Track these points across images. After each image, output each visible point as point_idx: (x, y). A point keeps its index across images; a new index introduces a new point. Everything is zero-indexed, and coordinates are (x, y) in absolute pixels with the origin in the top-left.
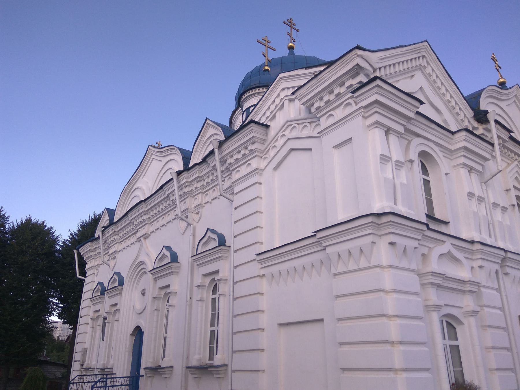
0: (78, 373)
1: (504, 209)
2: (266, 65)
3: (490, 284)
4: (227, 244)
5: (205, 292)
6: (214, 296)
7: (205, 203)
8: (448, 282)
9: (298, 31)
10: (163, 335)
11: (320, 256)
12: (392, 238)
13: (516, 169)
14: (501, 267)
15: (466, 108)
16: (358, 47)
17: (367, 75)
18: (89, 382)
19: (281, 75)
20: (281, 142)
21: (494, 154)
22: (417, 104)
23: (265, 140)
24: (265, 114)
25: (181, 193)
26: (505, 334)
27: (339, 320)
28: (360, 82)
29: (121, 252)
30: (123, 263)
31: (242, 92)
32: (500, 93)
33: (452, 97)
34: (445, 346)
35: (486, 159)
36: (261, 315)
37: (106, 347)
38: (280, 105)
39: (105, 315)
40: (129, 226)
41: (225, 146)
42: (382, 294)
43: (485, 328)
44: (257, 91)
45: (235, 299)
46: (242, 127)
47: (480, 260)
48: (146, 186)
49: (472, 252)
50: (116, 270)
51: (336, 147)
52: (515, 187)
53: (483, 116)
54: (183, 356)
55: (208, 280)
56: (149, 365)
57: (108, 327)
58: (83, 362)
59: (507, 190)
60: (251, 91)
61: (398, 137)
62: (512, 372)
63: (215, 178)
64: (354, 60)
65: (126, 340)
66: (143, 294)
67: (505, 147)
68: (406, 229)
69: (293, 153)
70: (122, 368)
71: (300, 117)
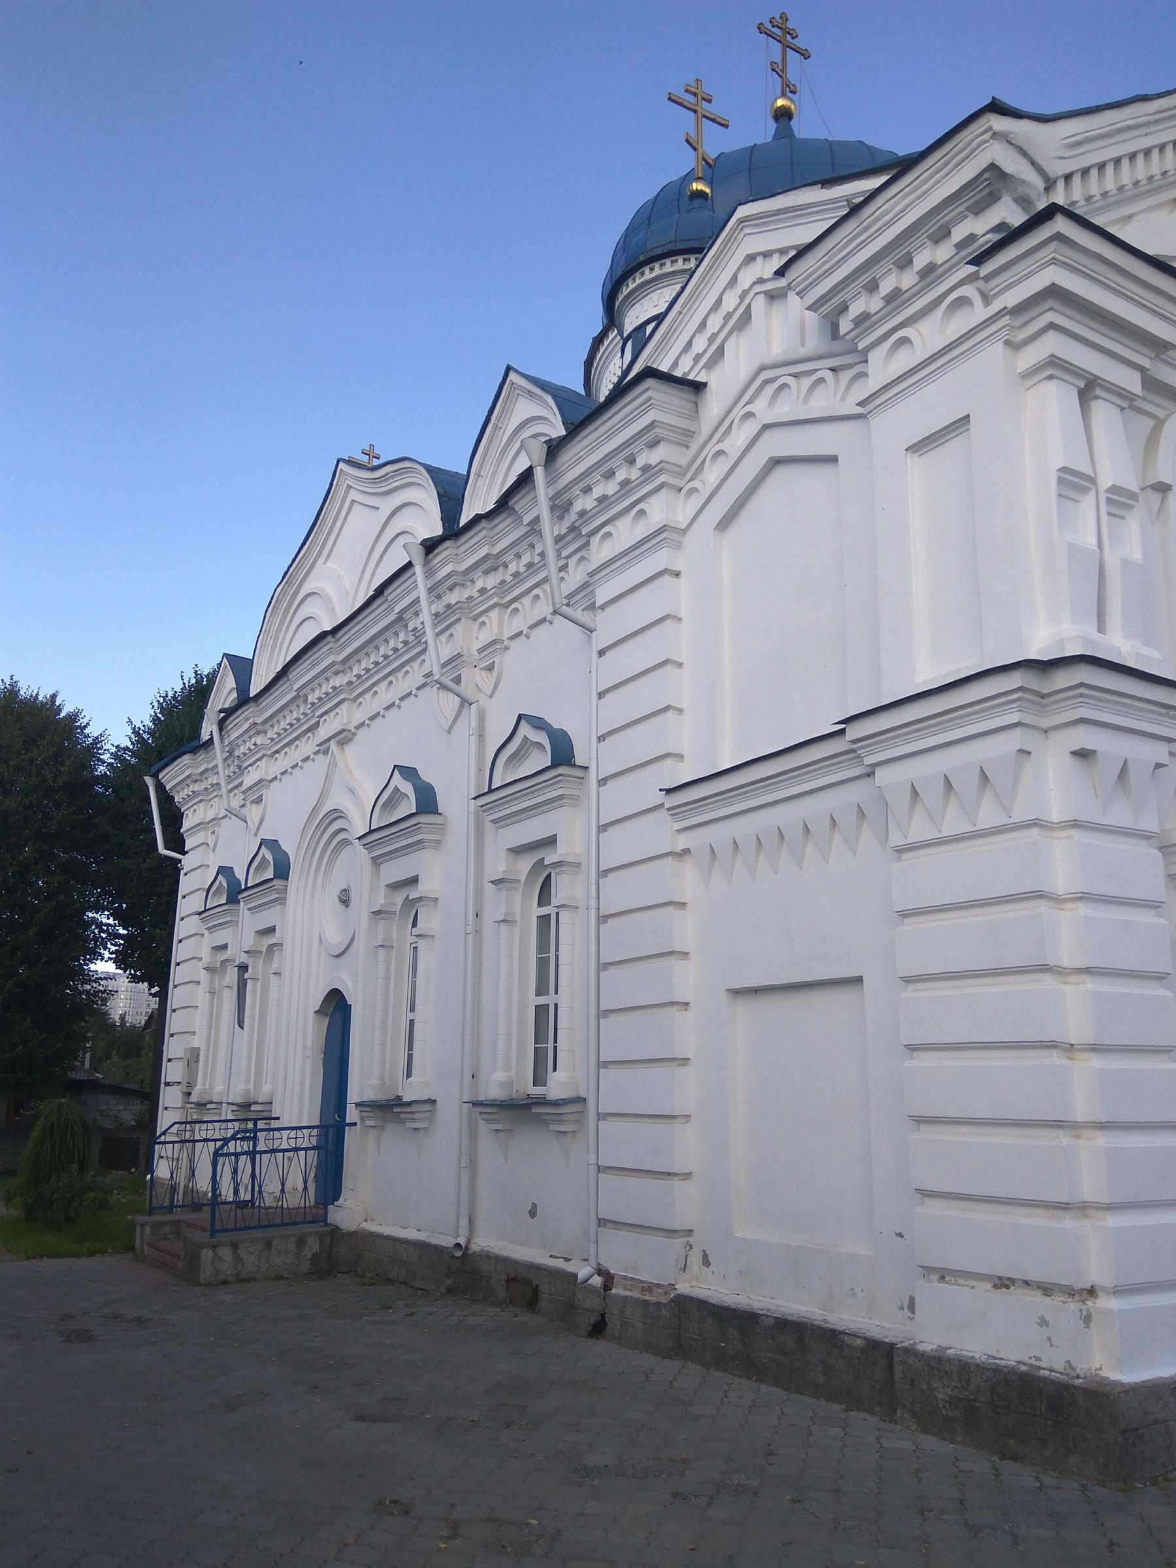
0: (176, 1116)
4: (579, 760)
6: (544, 911)
7: (512, 638)
9: (805, 55)
10: (404, 1017)
11: (857, 793)
12: (1084, 738)
16: (996, 107)
17: (1023, 202)
18: (206, 1140)
23: (690, 434)
24: (689, 344)
25: (439, 607)
27: (908, 980)
29: (276, 782)
30: (285, 813)
31: (619, 273)
36: (677, 964)
37: (250, 1044)
38: (736, 318)
39: (244, 958)
40: (293, 707)
41: (566, 456)
42: (1042, 906)
45: (602, 919)
46: (620, 391)
48: (337, 586)
50: (266, 834)
51: (919, 447)
55: (525, 865)
56: (370, 1095)
57: (254, 992)
58: (190, 1085)
60: (647, 270)
61: (1122, 409)
63: (537, 559)
65: (305, 1027)
66: (345, 901)
69: (780, 473)
70: (297, 1102)
71: (803, 352)
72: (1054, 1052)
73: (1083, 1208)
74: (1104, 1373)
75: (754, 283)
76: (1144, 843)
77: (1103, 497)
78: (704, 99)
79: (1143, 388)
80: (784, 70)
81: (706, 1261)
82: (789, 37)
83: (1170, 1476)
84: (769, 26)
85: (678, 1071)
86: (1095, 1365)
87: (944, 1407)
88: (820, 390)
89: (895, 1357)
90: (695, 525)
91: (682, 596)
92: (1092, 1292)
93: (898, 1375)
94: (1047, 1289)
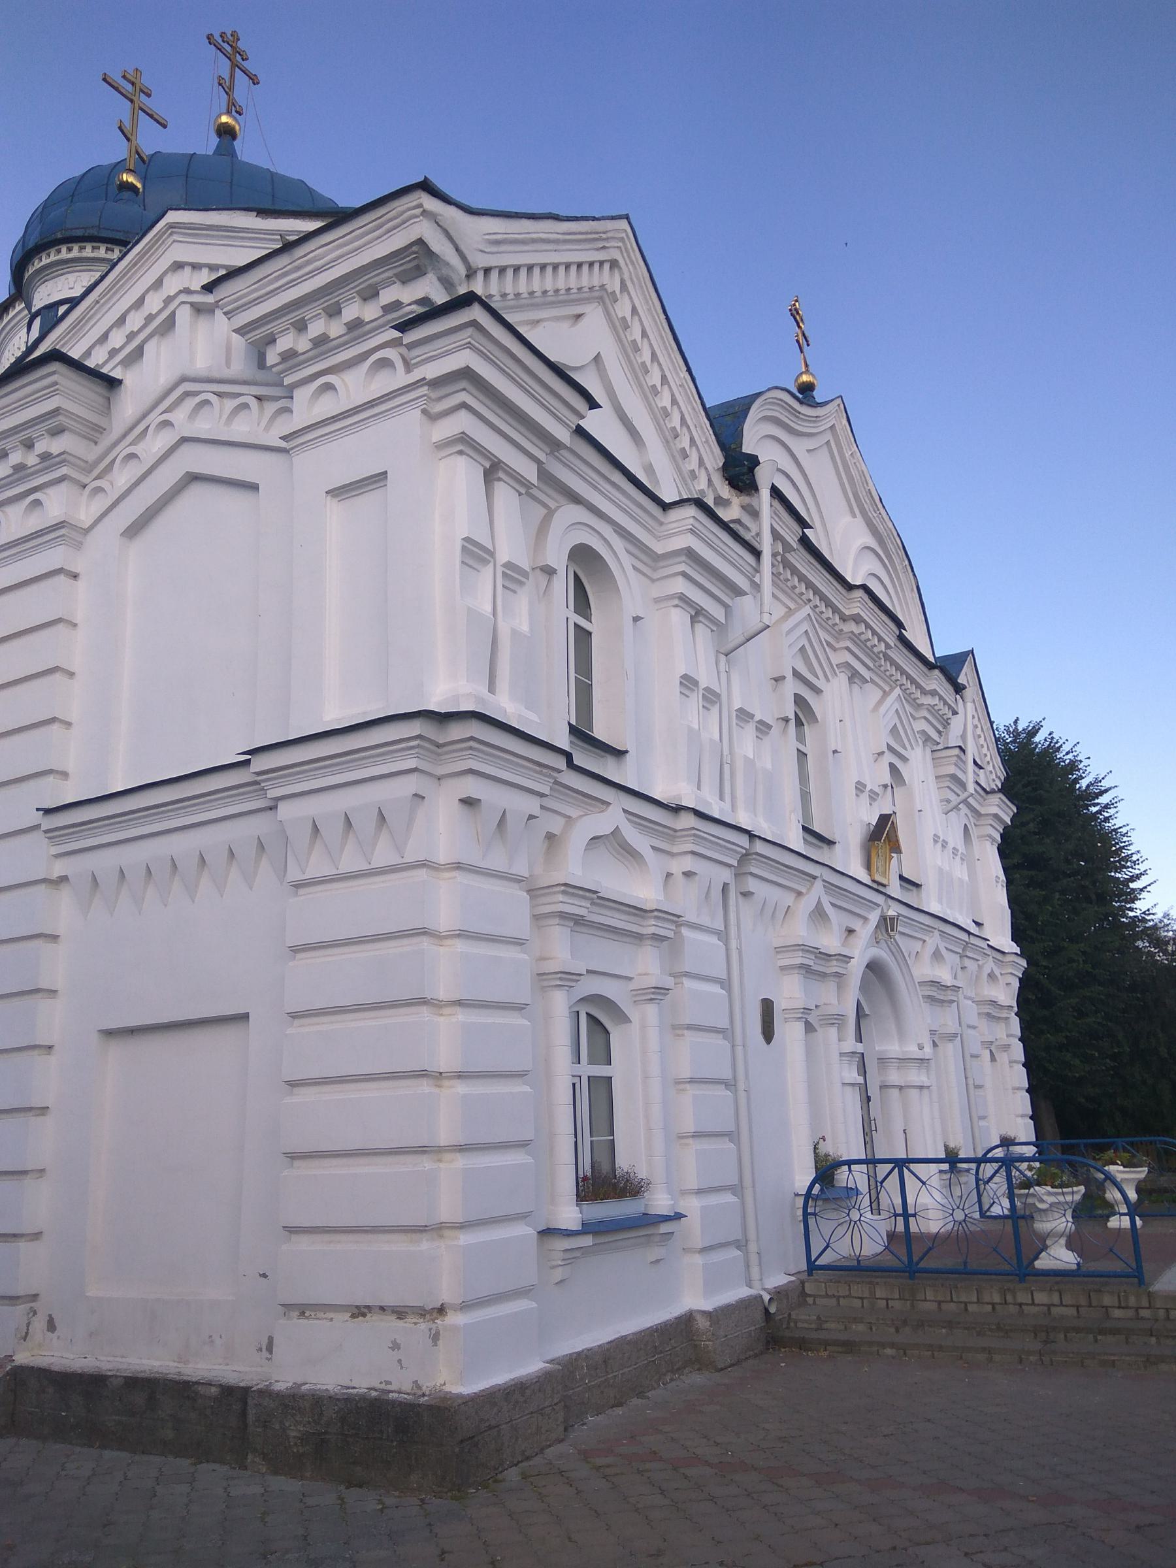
1: (763, 728)
2: (130, 171)
3: (705, 920)
9: (254, 80)
12: (471, 787)
13: (806, 626)
14: (737, 875)
15: (707, 441)
16: (426, 186)
17: (447, 283)
19: (172, 217)
20: (156, 444)
21: (757, 579)
22: (579, 404)
23: (100, 430)
31: (31, 245)
33: (674, 402)
34: (577, 1080)
36: (43, 1004)
38: (162, 317)
42: (425, 943)
44: (88, 252)
47: (689, 857)
49: (672, 834)
51: (340, 492)
52: (796, 674)
53: (745, 470)
59: (776, 680)
60: (64, 249)
61: (520, 494)
62: (731, 1141)
64: (412, 224)
67: (786, 564)
68: (512, 762)
69: (196, 489)
71: (227, 373)
72: (424, 1081)
73: (436, 1229)
74: (447, 1388)
75: (181, 292)
76: (516, 885)
77: (500, 570)
78: (141, 91)
79: (539, 478)
80: (231, 87)
81: (51, 1326)
82: (238, 58)
83: (500, 1477)
84: (220, 40)
85: (34, 1121)
86: (440, 1381)
87: (296, 1444)
88: (243, 414)
89: (250, 1402)
90: (99, 527)
91: (80, 600)
92: (441, 1310)
93: (251, 1418)
94: (400, 1313)
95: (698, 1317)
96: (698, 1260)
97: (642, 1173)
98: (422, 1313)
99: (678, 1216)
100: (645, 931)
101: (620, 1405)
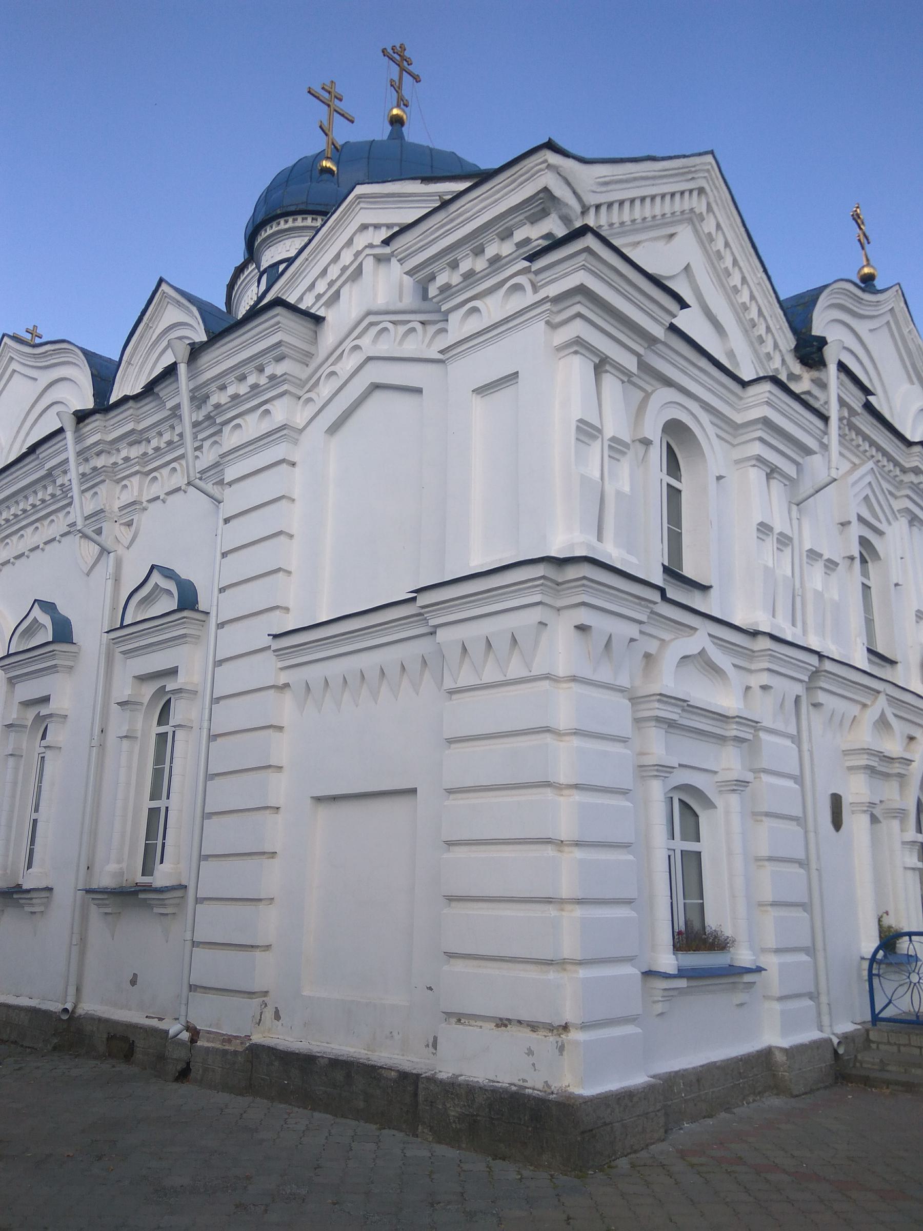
1: (831, 565)
2: (328, 158)
3: (780, 726)
4: (201, 607)
5: (140, 717)
6: (162, 729)
7: (149, 501)
8: (694, 717)
9: (417, 79)
10: (29, 815)
11: (422, 647)
12: (584, 616)
13: (869, 478)
14: (807, 689)
15: (781, 328)
16: (550, 146)
17: (566, 220)
19: (360, 190)
20: (349, 363)
21: (825, 440)
22: (672, 306)
23: (310, 355)
25: (86, 468)
26: (800, 830)
27: (450, 791)
28: (548, 236)
32: (860, 300)
33: (752, 297)
34: (671, 853)
35: (808, 451)
36: (273, 776)
38: (351, 268)
41: (206, 359)
42: (548, 738)
43: (759, 818)
44: (299, 223)
45: (212, 738)
46: (255, 313)
49: (751, 655)
51: (482, 390)
52: (861, 519)
53: (814, 349)
54: (78, 866)
55: (148, 691)
59: (842, 524)
60: (282, 221)
61: (623, 382)
63: (176, 439)
64: (540, 176)
67: (852, 426)
69: (378, 396)
72: (549, 847)
73: (560, 964)
74: (571, 1089)
76: (620, 694)
81: (277, 1016)
85: (266, 862)
88: (412, 336)
89: (421, 1086)
91: (296, 481)
92: (565, 1028)
93: (421, 1098)
94: (534, 1027)
95: (777, 1053)
96: (777, 1006)
97: (728, 932)
98: (551, 1028)
99: (759, 970)
100: (727, 734)
101: (710, 1116)
